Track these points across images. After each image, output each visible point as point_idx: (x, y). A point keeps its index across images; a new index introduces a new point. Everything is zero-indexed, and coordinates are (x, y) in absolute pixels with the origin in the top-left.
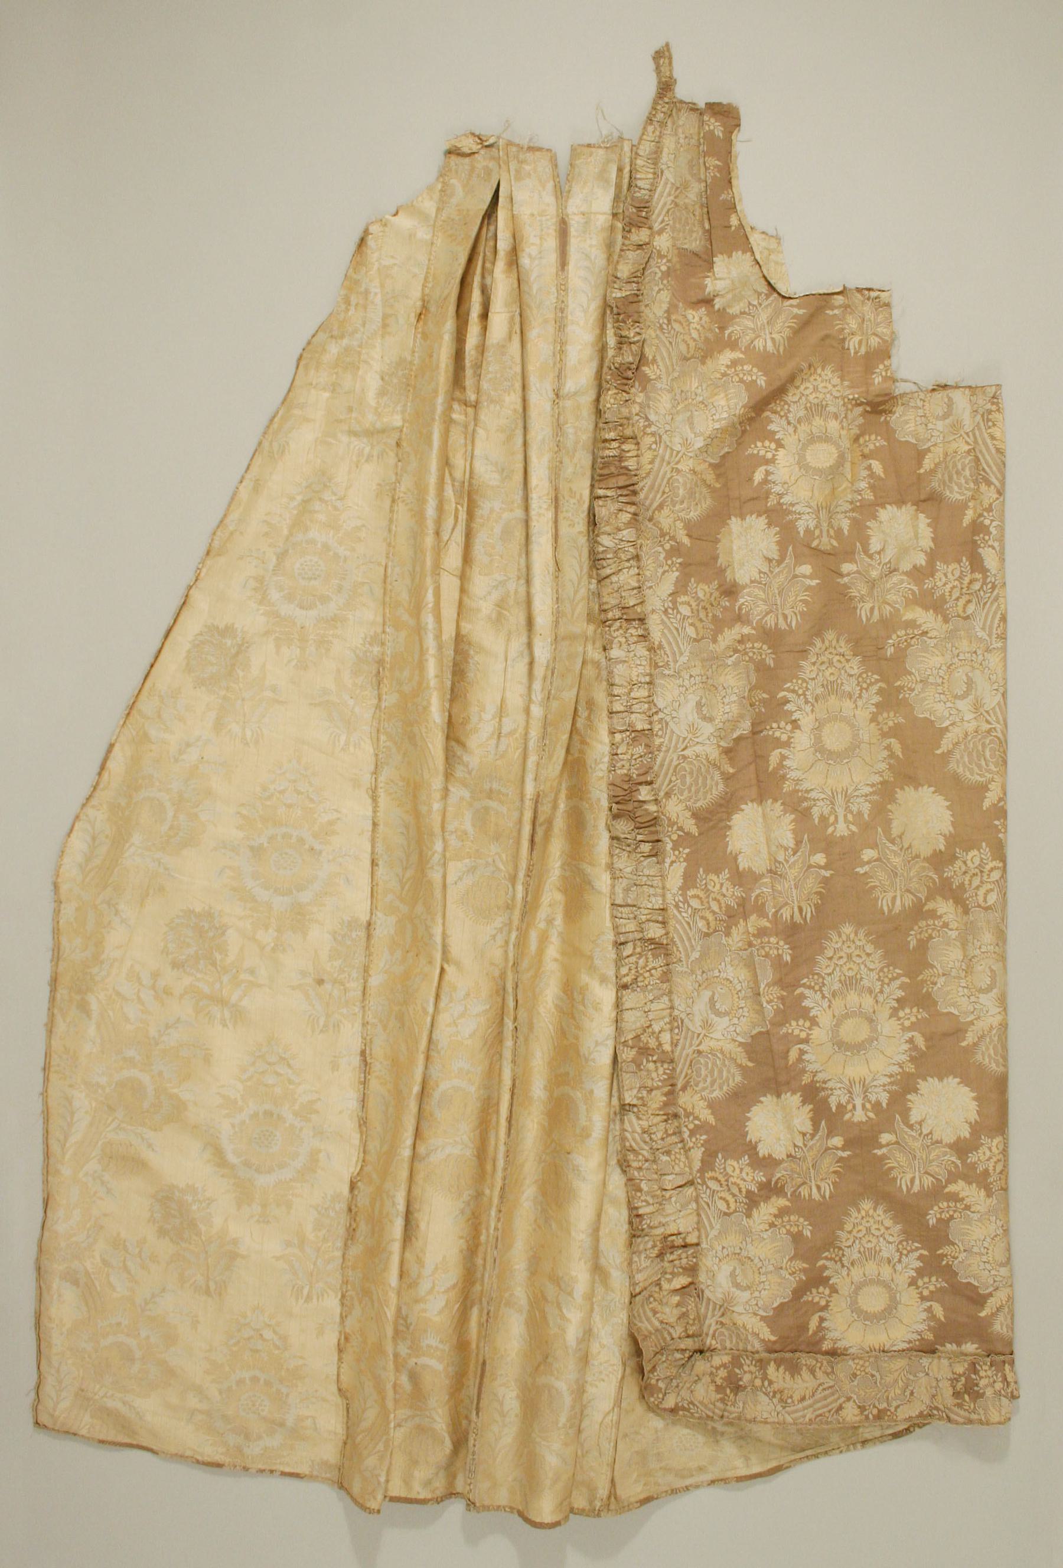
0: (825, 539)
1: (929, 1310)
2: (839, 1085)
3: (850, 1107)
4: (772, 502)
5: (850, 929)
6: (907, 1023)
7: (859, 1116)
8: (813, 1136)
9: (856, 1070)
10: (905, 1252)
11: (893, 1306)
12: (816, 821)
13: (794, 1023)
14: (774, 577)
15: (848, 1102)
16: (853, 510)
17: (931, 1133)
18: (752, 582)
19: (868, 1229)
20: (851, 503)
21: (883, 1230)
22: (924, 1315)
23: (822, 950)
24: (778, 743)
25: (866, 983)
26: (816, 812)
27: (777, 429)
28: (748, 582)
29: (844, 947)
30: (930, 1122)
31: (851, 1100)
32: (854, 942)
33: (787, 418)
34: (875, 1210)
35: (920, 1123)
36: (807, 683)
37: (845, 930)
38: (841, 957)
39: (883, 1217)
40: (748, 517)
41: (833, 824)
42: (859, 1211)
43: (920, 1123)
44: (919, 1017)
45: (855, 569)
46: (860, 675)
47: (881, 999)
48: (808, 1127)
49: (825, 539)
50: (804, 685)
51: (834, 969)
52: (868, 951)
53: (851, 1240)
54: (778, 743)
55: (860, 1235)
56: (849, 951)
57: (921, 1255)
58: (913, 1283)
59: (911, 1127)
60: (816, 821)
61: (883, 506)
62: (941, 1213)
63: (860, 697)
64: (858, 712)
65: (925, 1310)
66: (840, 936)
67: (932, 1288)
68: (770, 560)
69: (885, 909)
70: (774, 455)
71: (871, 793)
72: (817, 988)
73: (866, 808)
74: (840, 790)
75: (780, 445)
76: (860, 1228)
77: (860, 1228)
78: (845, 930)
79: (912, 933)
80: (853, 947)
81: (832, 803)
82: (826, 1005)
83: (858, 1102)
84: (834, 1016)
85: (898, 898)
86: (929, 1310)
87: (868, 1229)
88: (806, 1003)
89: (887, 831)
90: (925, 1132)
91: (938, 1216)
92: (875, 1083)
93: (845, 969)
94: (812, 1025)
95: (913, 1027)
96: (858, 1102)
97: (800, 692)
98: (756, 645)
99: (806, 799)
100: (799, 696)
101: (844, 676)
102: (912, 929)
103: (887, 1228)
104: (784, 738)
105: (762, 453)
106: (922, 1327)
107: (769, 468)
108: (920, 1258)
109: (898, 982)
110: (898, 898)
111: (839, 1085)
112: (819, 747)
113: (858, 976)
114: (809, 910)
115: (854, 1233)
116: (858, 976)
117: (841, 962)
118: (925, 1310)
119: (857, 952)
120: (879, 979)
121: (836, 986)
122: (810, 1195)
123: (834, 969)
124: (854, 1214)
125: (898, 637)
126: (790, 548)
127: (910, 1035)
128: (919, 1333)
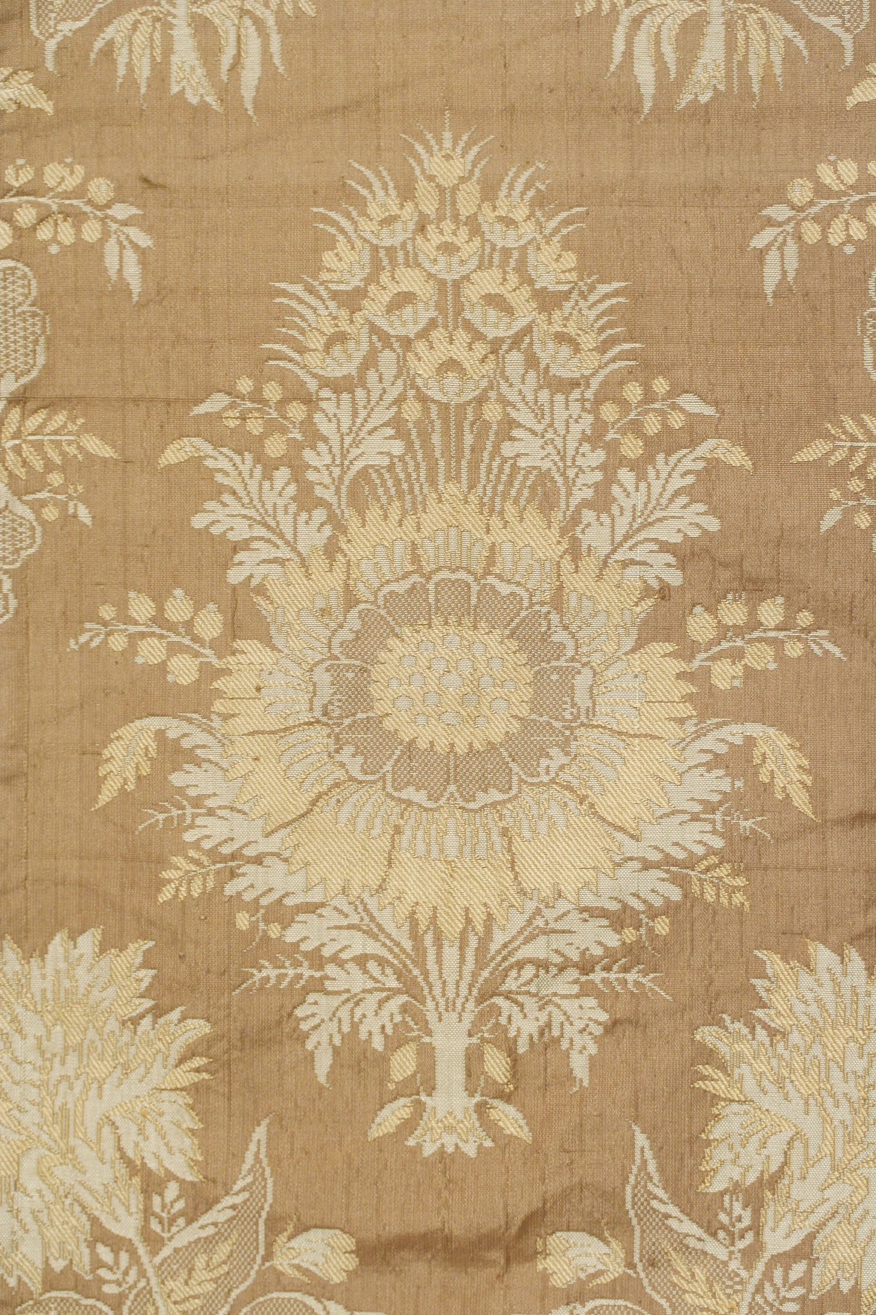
0: (451, 1099)
1: (739, 760)
2: (360, 944)
3: (403, 1064)
4: (180, 881)
5: (458, 167)
6: (725, 676)
7: (450, 1120)
8: (199, 1201)
9: (439, 874)
10: (632, 448)
11: (554, 721)
12: (323, 1064)
13: (141, 607)
14: (164, 1272)
15: (395, 1042)
16: (631, 956)
17: (805, 1251)
18: (51, 1281)
19: (450, 294)
20: (619, 919)
21: (526, 312)
22: (714, 784)
23: (307, 262)
24: (150, 694)
25: (529, 451)
26: (322, 1024)
27: (240, 531)
28: (35, 1284)
29: (428, 246)
30: (803, 1192)
31: (412, 1028)
32: (475, 230)
33: (298, 470)
34: (489, 192)
35: (758, 1193)
36: (310, 401)
37: (435, 164)
38: (405, 299)
39: (528, 230)
40: (57, 945)
41: (407, 1088)
42: (407, 192)
43: (758, 1193)
44: (794, 650)
45: (616, 1269)
46: (611, 391)
47: (596, 535)
48: (174, 1152)
49: (451, 1099)
50: (297, 411)
51: (370, 362)
52: (545, 281)
53: (359, 352)
54: (150, 694)
55: (407, 322)
56: (447, 269)
57: (713, 469)
58: (663, 619)
59: (706, 1213)
60: (323, 1064)
61: (792, 944)
62: (824, 221)
63: (602, 501)
64: (578, 582)
65: (716, 761)
66: (407, 192)
67: (761, 657)
68: (151, 1183)
69: (645, 73)
70: (209, 673)
71: (610, 959)
72: (275, 447)
73: (580, 1022)
74: (452, 927)
75: (244, 619)
76: (410, 280)
77: (410, 280)
78: (435, 164)
79: (779, 212)
80: (470, 249)
81: (410, 987)
82: (312, 534)
83: (450, 1040)
84: (350, 600)
85: (716, 31)
86: (739, 760)
87: (450, 294)
88: (219, 518)
89: (683, 1158)
90: (776, 1242)
91: (812, 233)
92: (537, 949)
93: (424, 363)
94: (235, 629)
95: (756, 699)
96: (450, 1040)
97: (275, 447)
98: (53, 174)
99: (270, 949)
100: (269, 467)
101: (520, 385)
102: (780, 196)
103: (548, 301)
104: (184, 670)
105: (151, 652)
106: (697, 838)
107: (174, 728)
108: (709, 484)
109: (690, 461)
110: (716, 31)
111: (360, 944)
112: (348, 712)
113: (492, 412)
114: (253, 45)
115: (374, 308)
116: (492, 412)
117: (407, 322)
118: (716, 761)
119: (487, 282)
120: (595, 437)
121: (378, 449)
122: (161, 73)
123: (370, 362)
124: (382, 200)
125: (821, 190)
126: (260, 1133)
127: (735, 733)
128: (677, 868)
